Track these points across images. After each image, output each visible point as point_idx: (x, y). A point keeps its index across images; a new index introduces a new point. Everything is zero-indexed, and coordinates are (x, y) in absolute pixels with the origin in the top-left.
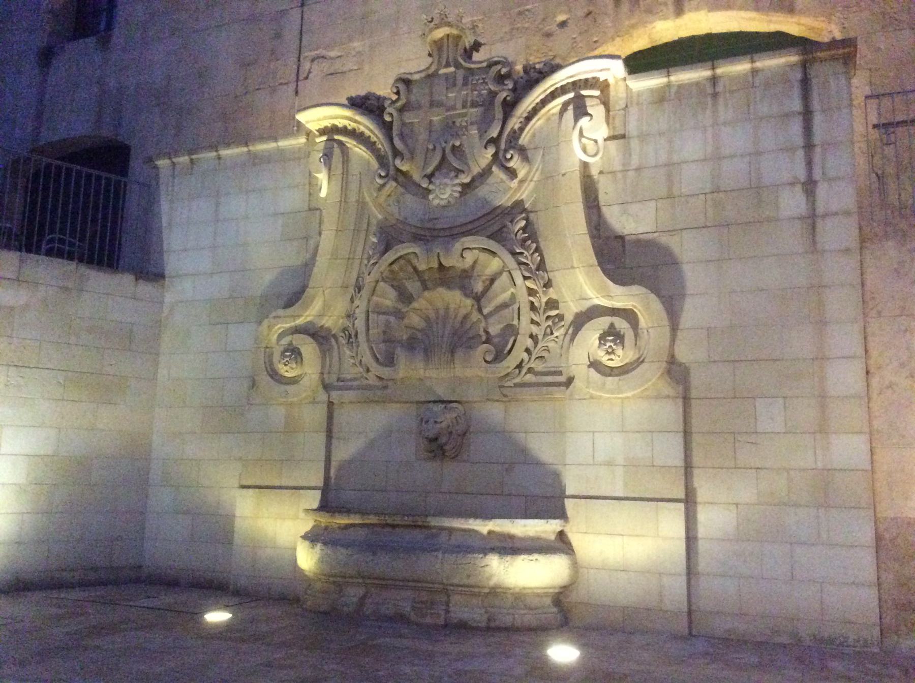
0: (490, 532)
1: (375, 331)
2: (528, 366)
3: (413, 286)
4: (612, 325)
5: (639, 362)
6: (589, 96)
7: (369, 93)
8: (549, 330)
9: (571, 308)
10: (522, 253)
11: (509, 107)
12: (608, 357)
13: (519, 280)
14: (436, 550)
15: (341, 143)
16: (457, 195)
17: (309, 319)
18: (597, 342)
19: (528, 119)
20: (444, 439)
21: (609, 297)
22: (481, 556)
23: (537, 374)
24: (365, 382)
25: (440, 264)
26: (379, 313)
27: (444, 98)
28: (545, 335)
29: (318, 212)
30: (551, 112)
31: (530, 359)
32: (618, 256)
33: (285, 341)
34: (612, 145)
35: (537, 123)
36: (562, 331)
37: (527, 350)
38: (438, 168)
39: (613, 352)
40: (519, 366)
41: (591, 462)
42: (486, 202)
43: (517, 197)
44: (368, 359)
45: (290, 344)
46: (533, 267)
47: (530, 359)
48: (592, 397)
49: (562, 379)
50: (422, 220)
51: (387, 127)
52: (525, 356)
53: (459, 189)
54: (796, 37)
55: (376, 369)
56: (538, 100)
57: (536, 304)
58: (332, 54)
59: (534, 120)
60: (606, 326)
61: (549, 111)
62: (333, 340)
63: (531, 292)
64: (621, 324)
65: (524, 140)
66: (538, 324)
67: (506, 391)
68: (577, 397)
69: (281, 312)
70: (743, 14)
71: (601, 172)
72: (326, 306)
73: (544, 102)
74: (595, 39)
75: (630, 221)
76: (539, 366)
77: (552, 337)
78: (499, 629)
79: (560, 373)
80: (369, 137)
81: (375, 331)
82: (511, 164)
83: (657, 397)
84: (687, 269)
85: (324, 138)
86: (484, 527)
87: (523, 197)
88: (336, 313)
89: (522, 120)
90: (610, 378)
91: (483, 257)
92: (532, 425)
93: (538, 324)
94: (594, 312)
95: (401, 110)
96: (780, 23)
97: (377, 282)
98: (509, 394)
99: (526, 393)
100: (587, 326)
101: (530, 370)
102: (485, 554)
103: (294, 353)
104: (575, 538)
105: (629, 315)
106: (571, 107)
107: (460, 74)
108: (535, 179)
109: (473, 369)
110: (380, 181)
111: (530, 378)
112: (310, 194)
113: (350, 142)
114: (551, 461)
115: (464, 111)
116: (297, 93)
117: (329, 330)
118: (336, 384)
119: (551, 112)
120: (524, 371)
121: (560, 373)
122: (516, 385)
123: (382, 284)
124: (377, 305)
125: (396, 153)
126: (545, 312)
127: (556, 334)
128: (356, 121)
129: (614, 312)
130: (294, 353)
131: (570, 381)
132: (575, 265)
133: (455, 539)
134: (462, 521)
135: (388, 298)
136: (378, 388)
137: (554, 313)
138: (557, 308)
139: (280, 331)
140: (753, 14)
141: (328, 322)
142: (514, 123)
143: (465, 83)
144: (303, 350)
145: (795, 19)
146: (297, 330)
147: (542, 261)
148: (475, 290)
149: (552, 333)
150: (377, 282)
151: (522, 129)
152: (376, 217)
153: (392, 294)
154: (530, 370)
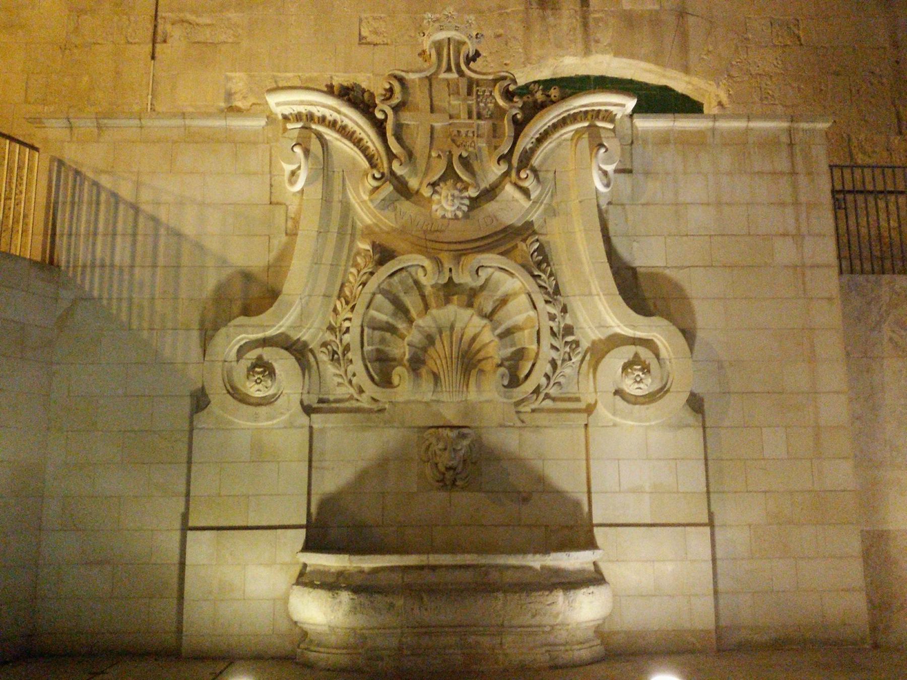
0: (543, 568)
1: (370, 348)
2: (545, 392)
3: (411, 302)
4: (636, 355)
5: (662, 391)
6: (604, 128)
7: (355, 84)
8: (567, 356)
9: (589, 334)
10: (539, 276)
11: (519, 126)
12: (636, 386)
13: (540, 304)
14: (498, 590)
15: (320, 136)
16: (465, 208)
17: (282, 330)
18: (620, 370)
19: (540, 141)
20: (466, 466)
21: (634, 327)
22: (547, 593)
23: (554, 399)
24: (355, 404)
25: (450, 279)
26: (374, 329)
27: (446, 105)
28: (564, 361)
29: (283, 207)
30: (565, 136)
31: (548, 384)
32: (636, 289)
33: (252, 355)
34: (622, 177)
35: (548, 145)
36: (579, 357)
37: (547, 377)
38: (443, 178)
39: (641, 381)
40: (537, 391)
41: (618, 490)
42: (494, 218)
43: (528, 218)
44: (362, 378)
45: (260, 358)
46: (551, 290)
47: (548, 384)
48: (615, 425)
49: (582, 405)
50: (425, 232)
51: (379, 126)
52: (544, 381)
53: (467, 202)
54: (677, 93)
55: (371, 389)
56: (550, 124)
57: (555, 329)
58: (201, 21)
59: (546, 144)
60: (631, 356)
61: (562, 135)
62: (310, 356)
63: (552, 318)
64: (645, 354)
65: (536, 161)
66: (557, 349)
67: (522, 416)
68: (600, 424)
69: (242, 320)
70: (643, 65)
71: (610, 203)
72: (304, 316)
73: (555, 127)
74: (507, 62)
75: (646, 256)
76: (553, 391)
77: (570, 363)
78: (561, 667)
79: (578, 400)
80: (354, 132)
81: (370, 348)
82: (526, 184)
83: (679, 427)
84: (695, 303)
85: (299, 125)
86: (536, 562)
87: (534, 218)
88: (316, 325)
89: (533, 140)
90: (637, 406)
91: (498, 275)
92: (552, 452)
93: (557, 349)
94: (616, 341)
95: (396, 109)
96: (671, 78)
97: (374, 294)
98: (525, 420)
99: (542, 419)
100: (612, 353)
101: (547, 396)
102: (551, 591)
103: (265, 369)
104: (607, 570)
105: (647, 343)
106: (586, 136)
107: (463, 84)
108: (545, 202)
109: (487, 395)
110: (375, 184)
111: (548, 403)
112: (271, 186)
113: (330, 135)
114: (570, 490)
115: (470, 121)
116: (153, 58)
117: (305, 344)
118: (316, 405)
119: (563, 137)
120: (542, 396)
121: (578, 400)
122: (533, 411)
123: (379, 297)
124: (373, 319)
125: (391, 156)
126: (563, 336)
127: (574, 360)
128: (339, 112)
129: (635, 341)
130: (265, 369)
131: (590, 410)
132: (594, 292)
133: (509, 577)
134: (520, 557)
135: (383, 314)
136: (370, 411)
137: (569, 339)
138: (572, 334)
139: (242, 343)
140: (651, 66)
141: (305, 335)
142: (525, 142)
143: (469, 93)
144: (276, 365)
145: (687, 79)
146: (265, 342)
147: (557, 285)
148: (485, 309)
149: (570, 359)
150: (374, 294)
151: (533, 151)
152: (362, 221)
153: (389, 306)
154: (547, 396)
